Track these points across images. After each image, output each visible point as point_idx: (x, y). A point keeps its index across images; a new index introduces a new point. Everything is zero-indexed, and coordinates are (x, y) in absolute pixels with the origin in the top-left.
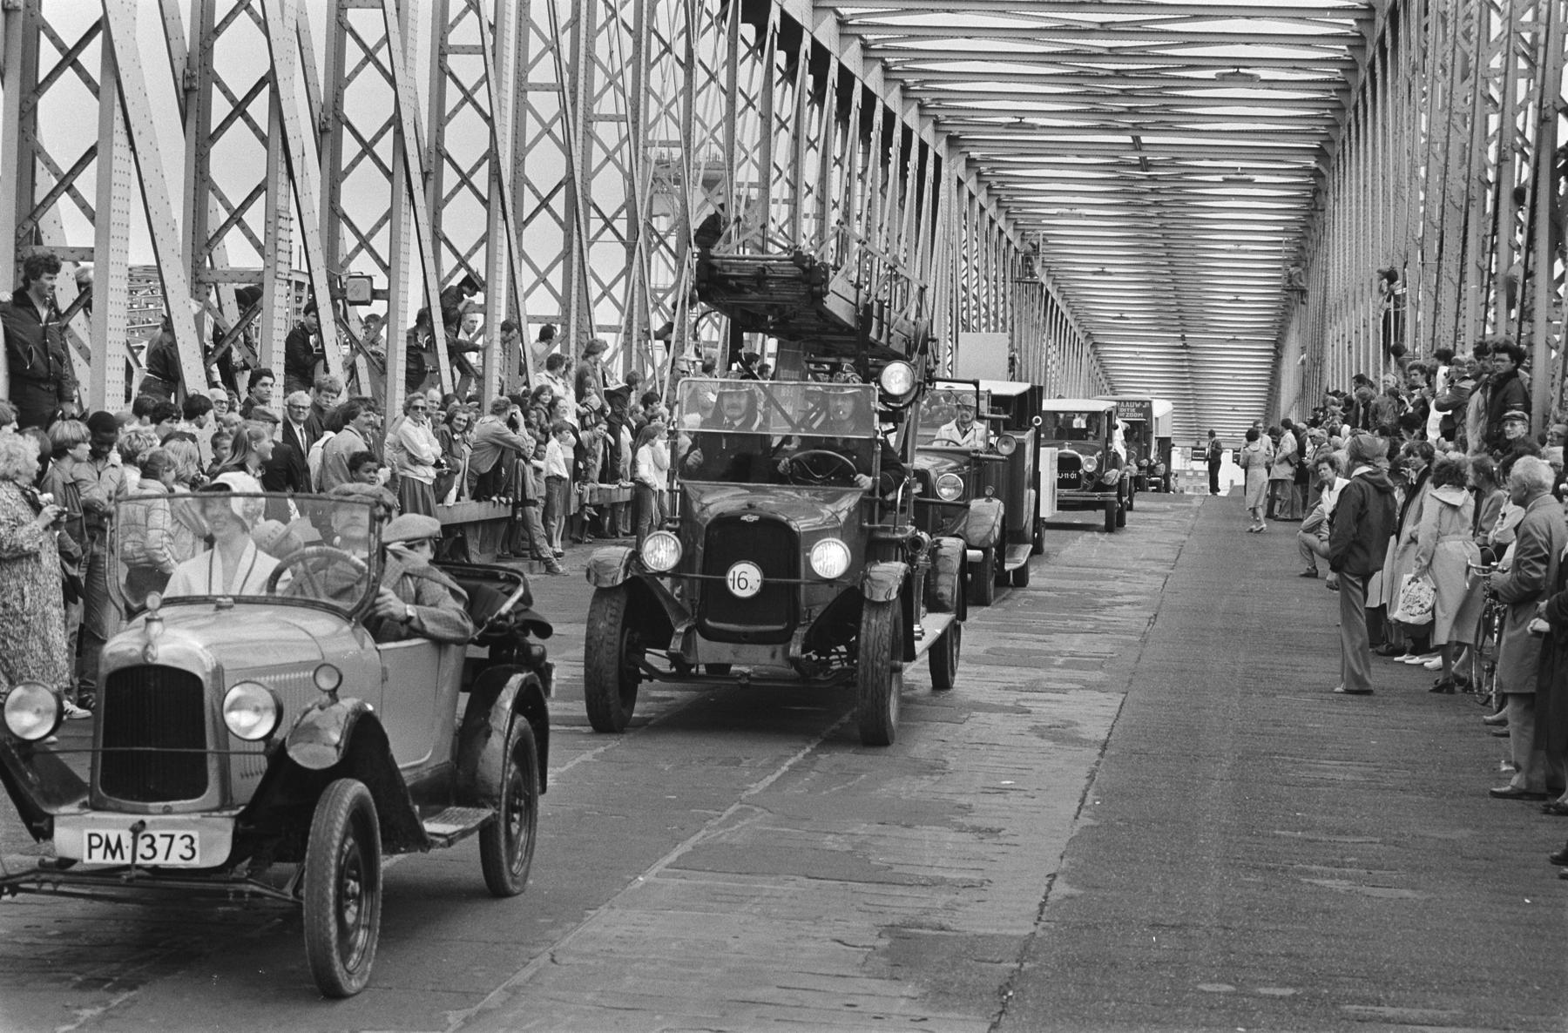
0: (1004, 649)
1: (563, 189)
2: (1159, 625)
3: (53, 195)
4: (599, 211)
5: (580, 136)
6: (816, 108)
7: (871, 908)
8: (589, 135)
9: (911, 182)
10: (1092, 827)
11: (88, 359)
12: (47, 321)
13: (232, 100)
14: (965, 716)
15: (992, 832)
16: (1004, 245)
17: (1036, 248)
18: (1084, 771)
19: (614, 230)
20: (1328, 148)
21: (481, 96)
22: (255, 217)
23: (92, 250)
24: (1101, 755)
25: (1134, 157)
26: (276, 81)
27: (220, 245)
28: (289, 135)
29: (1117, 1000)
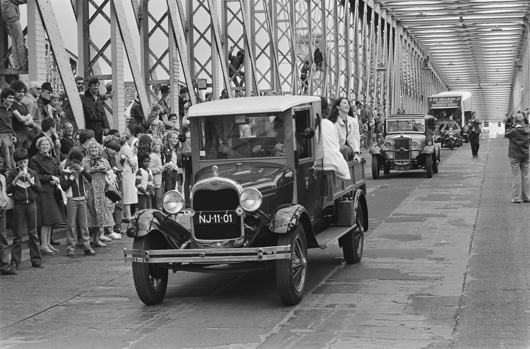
0: (433, 195)
1: (269, 46)
2: (485, 183)
3: (96, 58)
4: (281, 53)
5: (273, 27)
6: (352, 14)
7: (404, 289)
8: (277, 27)
9: (385, 37)
10: (476, 256)
11: (112, 113)
12: (97, 101)
13: (155, 21)
14: (424, 219)
15: (441, 259)
16: (417, 57)
17: (428, 57)
18: (469, 236)
19: (287, 59)
20: (527, 17)
21: (240, 16)
22: (166, 61)
23: (111, 76)
24: (474, 230)
25: (461, 24)
26: (170, 14)
27: (154, 72)
28: (176, 32)
29: (497, 318)
